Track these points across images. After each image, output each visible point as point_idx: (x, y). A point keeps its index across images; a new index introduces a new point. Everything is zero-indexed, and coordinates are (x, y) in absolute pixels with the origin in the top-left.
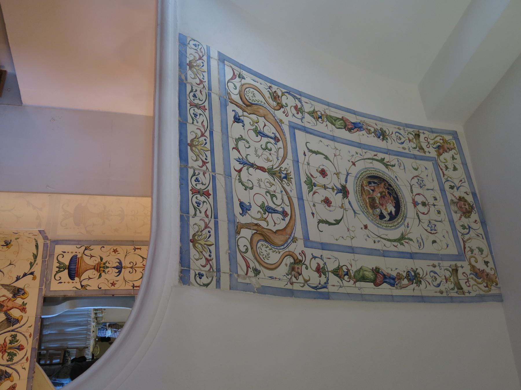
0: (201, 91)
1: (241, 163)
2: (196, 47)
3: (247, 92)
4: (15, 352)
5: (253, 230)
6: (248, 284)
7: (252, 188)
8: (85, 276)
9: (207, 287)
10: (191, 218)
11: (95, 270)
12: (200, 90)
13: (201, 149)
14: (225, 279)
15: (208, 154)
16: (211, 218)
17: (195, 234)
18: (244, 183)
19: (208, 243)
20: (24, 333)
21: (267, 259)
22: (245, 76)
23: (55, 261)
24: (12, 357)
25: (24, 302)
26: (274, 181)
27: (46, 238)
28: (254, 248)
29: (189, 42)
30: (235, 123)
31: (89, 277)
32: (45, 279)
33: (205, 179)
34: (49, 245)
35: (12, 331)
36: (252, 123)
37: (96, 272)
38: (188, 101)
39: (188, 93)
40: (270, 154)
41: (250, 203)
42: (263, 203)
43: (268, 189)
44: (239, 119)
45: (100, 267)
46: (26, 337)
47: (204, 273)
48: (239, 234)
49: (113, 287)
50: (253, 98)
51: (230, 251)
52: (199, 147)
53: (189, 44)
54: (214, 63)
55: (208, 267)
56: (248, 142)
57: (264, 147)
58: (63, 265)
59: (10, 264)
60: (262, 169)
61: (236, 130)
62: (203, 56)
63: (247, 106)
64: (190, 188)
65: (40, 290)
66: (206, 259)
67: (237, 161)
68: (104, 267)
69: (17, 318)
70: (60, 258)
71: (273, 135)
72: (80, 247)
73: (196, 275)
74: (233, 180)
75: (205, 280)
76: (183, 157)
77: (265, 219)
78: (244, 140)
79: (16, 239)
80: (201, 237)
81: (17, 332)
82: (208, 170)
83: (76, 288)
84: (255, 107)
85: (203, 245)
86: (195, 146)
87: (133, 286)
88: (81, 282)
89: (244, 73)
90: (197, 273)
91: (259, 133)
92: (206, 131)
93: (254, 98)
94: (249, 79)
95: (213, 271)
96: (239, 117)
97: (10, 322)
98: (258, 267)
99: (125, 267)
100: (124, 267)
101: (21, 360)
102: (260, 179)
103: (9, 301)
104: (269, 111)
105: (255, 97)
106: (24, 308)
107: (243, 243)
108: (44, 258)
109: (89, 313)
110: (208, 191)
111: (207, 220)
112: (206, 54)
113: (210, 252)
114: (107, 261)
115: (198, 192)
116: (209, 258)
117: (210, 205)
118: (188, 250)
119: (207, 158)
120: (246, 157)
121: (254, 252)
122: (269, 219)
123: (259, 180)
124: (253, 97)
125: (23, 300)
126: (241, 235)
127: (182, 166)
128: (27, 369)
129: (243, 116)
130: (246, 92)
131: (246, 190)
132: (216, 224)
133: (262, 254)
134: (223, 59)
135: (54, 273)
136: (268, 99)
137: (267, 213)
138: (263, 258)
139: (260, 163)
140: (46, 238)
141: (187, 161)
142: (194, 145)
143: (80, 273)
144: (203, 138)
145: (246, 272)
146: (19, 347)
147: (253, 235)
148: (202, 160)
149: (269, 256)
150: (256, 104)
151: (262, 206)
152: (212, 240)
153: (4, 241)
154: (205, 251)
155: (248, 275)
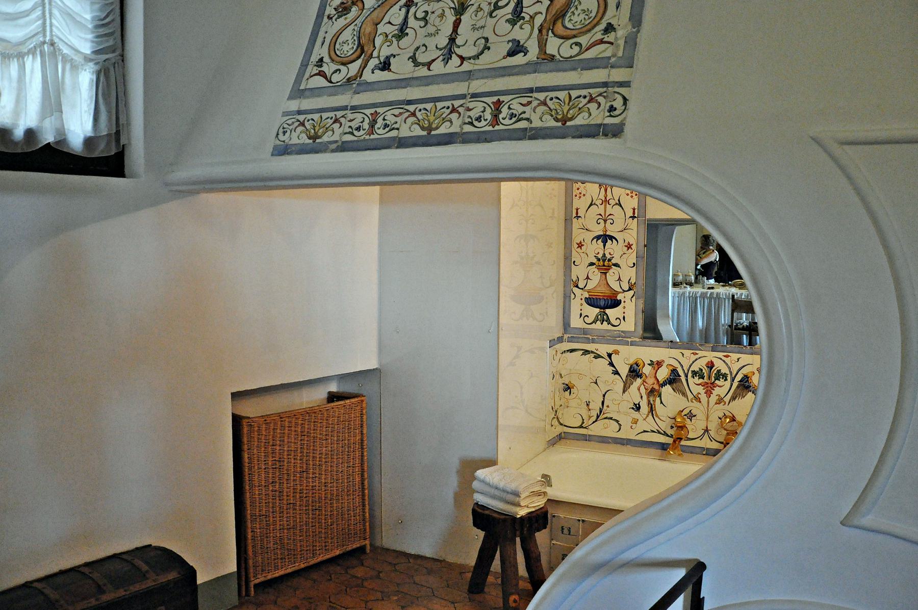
0: (351, 121)
1: (449, 57)
2: (287, 131)
3: (342, 53)
4: (715, 372)
5: (548, 36)
6: (625, 42)
7: (487, 40)
8: (615, 286)
9: (628, 100)
10: (533, 125)
11: (607, 273)
12: (349, 121)
13: (434, 116)
14: (618, 75)
15: (440, 105)
16: (531, 97)
17: (554, 119)
18: (479, 51)
19: (567, 101)
20: (691, 362)
21: (591, 13)
22: (319, 57)
23: (593, 326)
24: (721, 374)
25: (649, 364)
26: (473, 5)
27: (560, 340)
28: (573, 33)
29: (281, 141)
30: (390, 69)
31: (618, 280)
32: (618, 339)
33: (477, 107)
34: (570, 336)
35: (687, 376)
36: (388, 44)
37: (611, 271)
38: (367, 137)
39: (356, 139)
40: (433, 12)
41: (509, 41)
42: (507, 21)
43: (486, 14)
44: (385, 62)
45: (604, 265)
46: (696, 360)
47: (609, 104)
48: (554, 56)
49: (634, 247)
50: (350, 44)
51: (577, 69)
52: (432, 118)
53: (284, 141)
55: (600, 99)
56: (418, 48)
57: (422, 23)
58: (599, 316)
59: (596, 383)
60: (457, 24)
61: (402, 67)
62: (298, 121)
63: (363, 51)
64: (491, 128)
65: (633, 344)
66: (589, 102)
67: (447, 63)
68: (604, 261)
69: (670, 371)
70: (589, 320)
71: (404, 10)
72: (574, 294)
73: (611, 116)
74: (476, 67)
75: (618, 103)
76: (448, 140)
77: (531, 17)
78: (415, 54)
79: (562, 377)
80: (558, 111)
81: (688, 371)
82: (463, 104)
83: (632, 297)
84: (363, 41)
85: (569, 107)
87: (633, 217)
88: (624, 291)
89: (314, 58)
90: (608, 114)
91: (402, 32)
92: (407, 110)
93: (350, 42)
94: (321, 51)
95: (605, 92)
96: (381, 63)
97: (674, 379)
98: (603, 26)
99: (605, 230)
100: (604, 232)
101: (727, 364)
102: (472, 27)
103: (646, 382)
104: (366, 18)
105: (348, 40)
106: (657, 363)
107: (568, 50)
108: (588, 341)
109: (677, 295)
110: (493, 103)
111: (535, 103)
112: (294, 117)
114: (595, 256)
115: (496, 116)
116: (450, 109)
117: (512, 99)
118: (577, 127)
119: (446, 106)
120: (441, 49)
121: (581, 33)
122: (531, 11)
123: (474, 28)
124: (348, 44)
125: (646, 365)
126: (555, 53)
127: (460, 141)
128: (739, 355)
129: (378, 57)
130: (342, 54)
131: (489, 48)
132: (540, 90)
133: (583, 21)
134: (298, 93)
135: (610, 327)
136: (348, 20)
137: (523, 15)
138: (589, 18)
139: (447, 28)
140: (560, 340)
141: (452, 135)
143: (611, 293)
144: (418, 114)
145: (609, 45)
146: (709, 367)
147: (555, 35)
148: (449, 114)
149: (586, 10)
150: (359, 38)
151: (513, 22)
152: (562, 95)
153: (565, 391)
154: (579, 104)
155: (612, 41)
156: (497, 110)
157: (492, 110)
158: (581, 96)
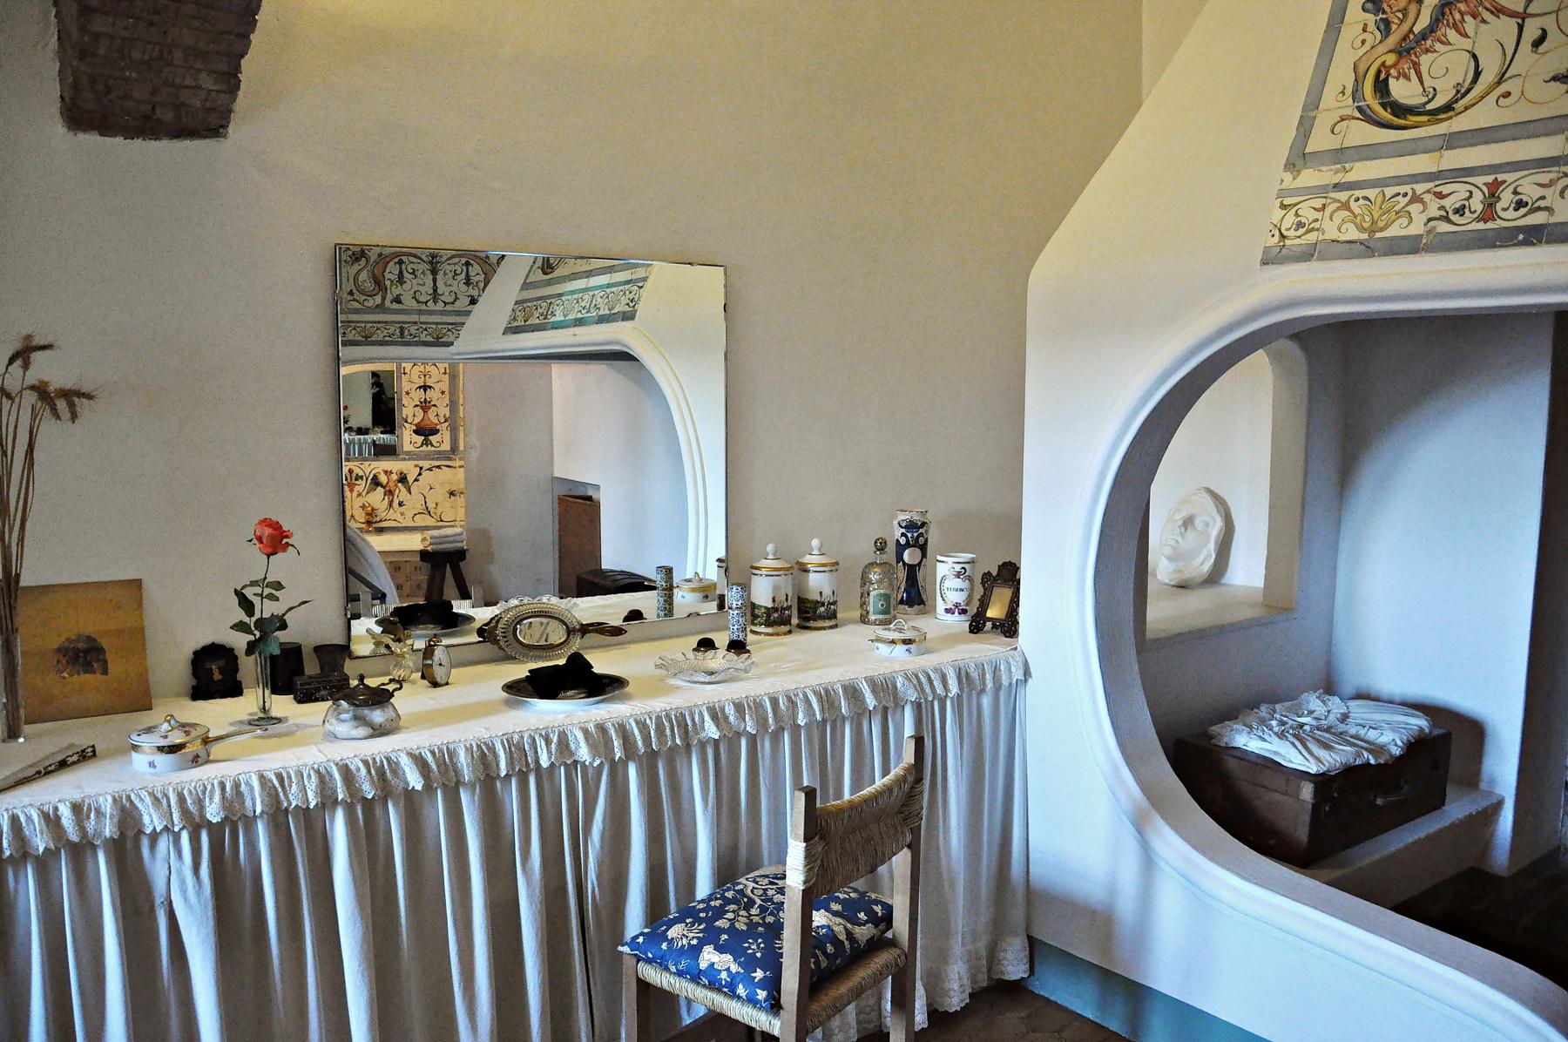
10: (1327, 236)
13: (1381, 208)
33: (1457, 193)
38: (1481, 226)
54: (1309, 178)
55: (1427, 197)
68: (425, 403)
86: (1374, 222)
87: (445, 373)
113: (1398, 194)
135: (433, 449)
142: (1372, 225)
148: (1407, 205)
156: (1493, 196)
157: (1485, 196)
158: (1400, 194)
